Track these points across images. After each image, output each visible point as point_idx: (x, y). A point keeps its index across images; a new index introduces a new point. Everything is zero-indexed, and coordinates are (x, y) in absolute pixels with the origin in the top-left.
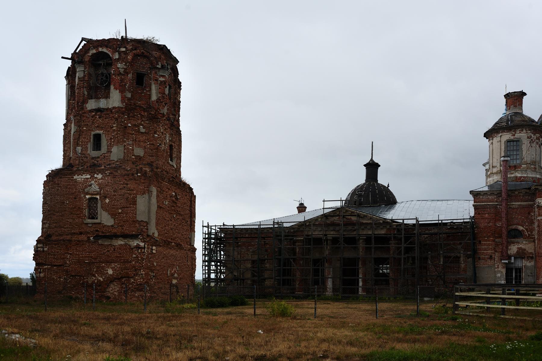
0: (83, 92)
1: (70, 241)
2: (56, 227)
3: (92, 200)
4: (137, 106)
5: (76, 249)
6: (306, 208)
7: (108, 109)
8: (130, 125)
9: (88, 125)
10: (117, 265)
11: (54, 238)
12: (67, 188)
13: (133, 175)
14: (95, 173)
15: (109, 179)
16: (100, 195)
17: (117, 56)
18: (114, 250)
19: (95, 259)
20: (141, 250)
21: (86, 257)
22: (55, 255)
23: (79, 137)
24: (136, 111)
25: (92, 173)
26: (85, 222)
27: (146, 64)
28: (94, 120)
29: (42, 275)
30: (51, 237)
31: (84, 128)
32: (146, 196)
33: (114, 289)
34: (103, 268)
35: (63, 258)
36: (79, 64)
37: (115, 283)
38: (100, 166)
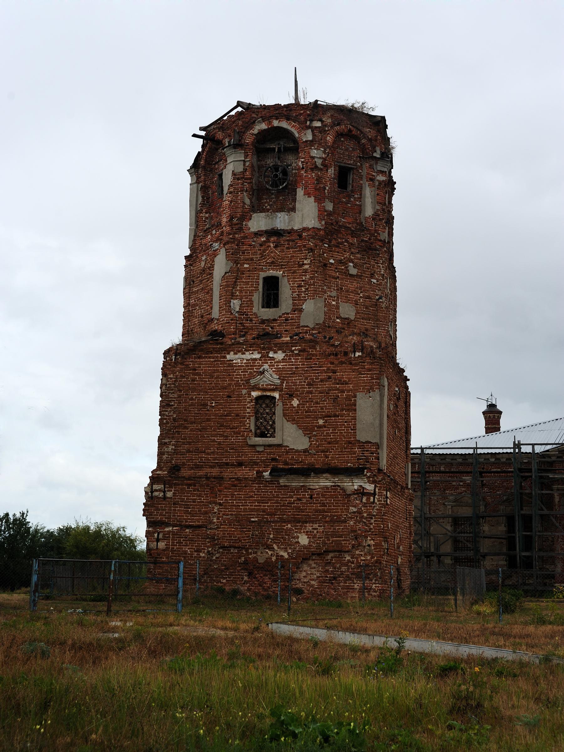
0: (243, 198)
1: (220, 479)
2: (189, 451)
3: (265, 401)
4: (340, 227)
5: (232, 495)
6: (501, 413)
7: (290, 232)
8: (332, 261)
9: (252, 259)
10: (317, 528)
11: (185, 472)
12: (212, 377)
13: (346, 354)
14: (271, 349)
15: (298, 362)
16: (281, 390)
17: (309, 136)
18: (311, 498)
19: (272, 514)
20: (368, 499)
21: (252, 510)
22: (187, 506)
23: (235, 282)
24: (339, 235)
25: (264, 349)
26: (250, 442)
27: (354, 149)
28: (264, 251)
29: (162, 545)
30: (179, 470)
31: (246, 266)
32: (376, 394)
33: (309, 575)
34: (288, 532)
35: (206, 513)
36: (235, 148)
37: (310, 562)
38: (277, 336)
